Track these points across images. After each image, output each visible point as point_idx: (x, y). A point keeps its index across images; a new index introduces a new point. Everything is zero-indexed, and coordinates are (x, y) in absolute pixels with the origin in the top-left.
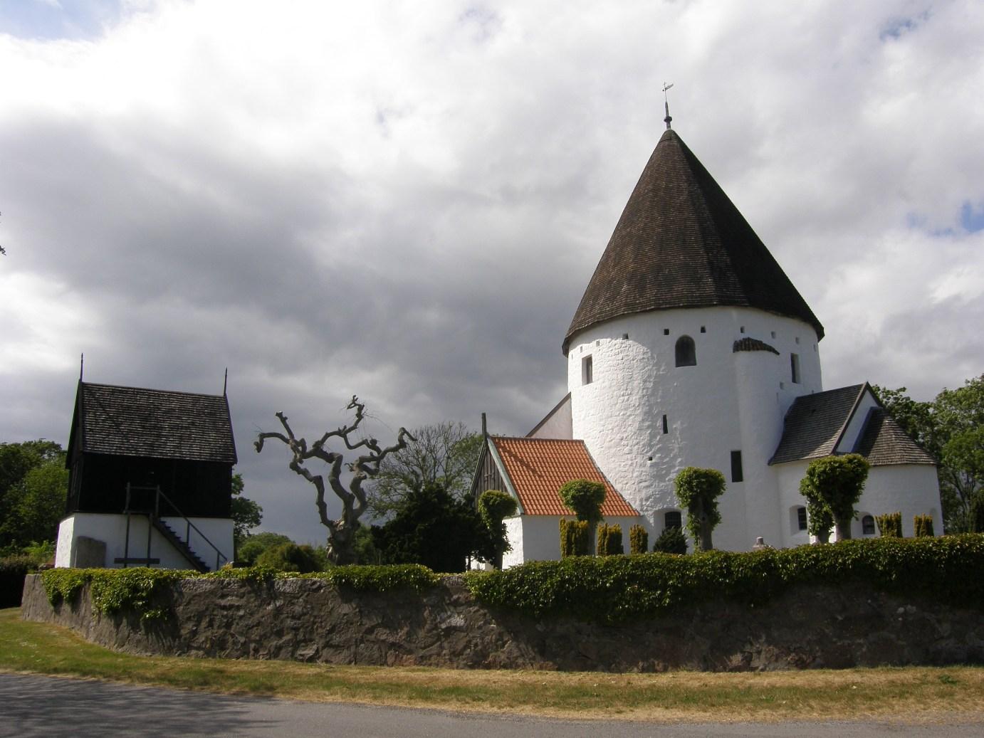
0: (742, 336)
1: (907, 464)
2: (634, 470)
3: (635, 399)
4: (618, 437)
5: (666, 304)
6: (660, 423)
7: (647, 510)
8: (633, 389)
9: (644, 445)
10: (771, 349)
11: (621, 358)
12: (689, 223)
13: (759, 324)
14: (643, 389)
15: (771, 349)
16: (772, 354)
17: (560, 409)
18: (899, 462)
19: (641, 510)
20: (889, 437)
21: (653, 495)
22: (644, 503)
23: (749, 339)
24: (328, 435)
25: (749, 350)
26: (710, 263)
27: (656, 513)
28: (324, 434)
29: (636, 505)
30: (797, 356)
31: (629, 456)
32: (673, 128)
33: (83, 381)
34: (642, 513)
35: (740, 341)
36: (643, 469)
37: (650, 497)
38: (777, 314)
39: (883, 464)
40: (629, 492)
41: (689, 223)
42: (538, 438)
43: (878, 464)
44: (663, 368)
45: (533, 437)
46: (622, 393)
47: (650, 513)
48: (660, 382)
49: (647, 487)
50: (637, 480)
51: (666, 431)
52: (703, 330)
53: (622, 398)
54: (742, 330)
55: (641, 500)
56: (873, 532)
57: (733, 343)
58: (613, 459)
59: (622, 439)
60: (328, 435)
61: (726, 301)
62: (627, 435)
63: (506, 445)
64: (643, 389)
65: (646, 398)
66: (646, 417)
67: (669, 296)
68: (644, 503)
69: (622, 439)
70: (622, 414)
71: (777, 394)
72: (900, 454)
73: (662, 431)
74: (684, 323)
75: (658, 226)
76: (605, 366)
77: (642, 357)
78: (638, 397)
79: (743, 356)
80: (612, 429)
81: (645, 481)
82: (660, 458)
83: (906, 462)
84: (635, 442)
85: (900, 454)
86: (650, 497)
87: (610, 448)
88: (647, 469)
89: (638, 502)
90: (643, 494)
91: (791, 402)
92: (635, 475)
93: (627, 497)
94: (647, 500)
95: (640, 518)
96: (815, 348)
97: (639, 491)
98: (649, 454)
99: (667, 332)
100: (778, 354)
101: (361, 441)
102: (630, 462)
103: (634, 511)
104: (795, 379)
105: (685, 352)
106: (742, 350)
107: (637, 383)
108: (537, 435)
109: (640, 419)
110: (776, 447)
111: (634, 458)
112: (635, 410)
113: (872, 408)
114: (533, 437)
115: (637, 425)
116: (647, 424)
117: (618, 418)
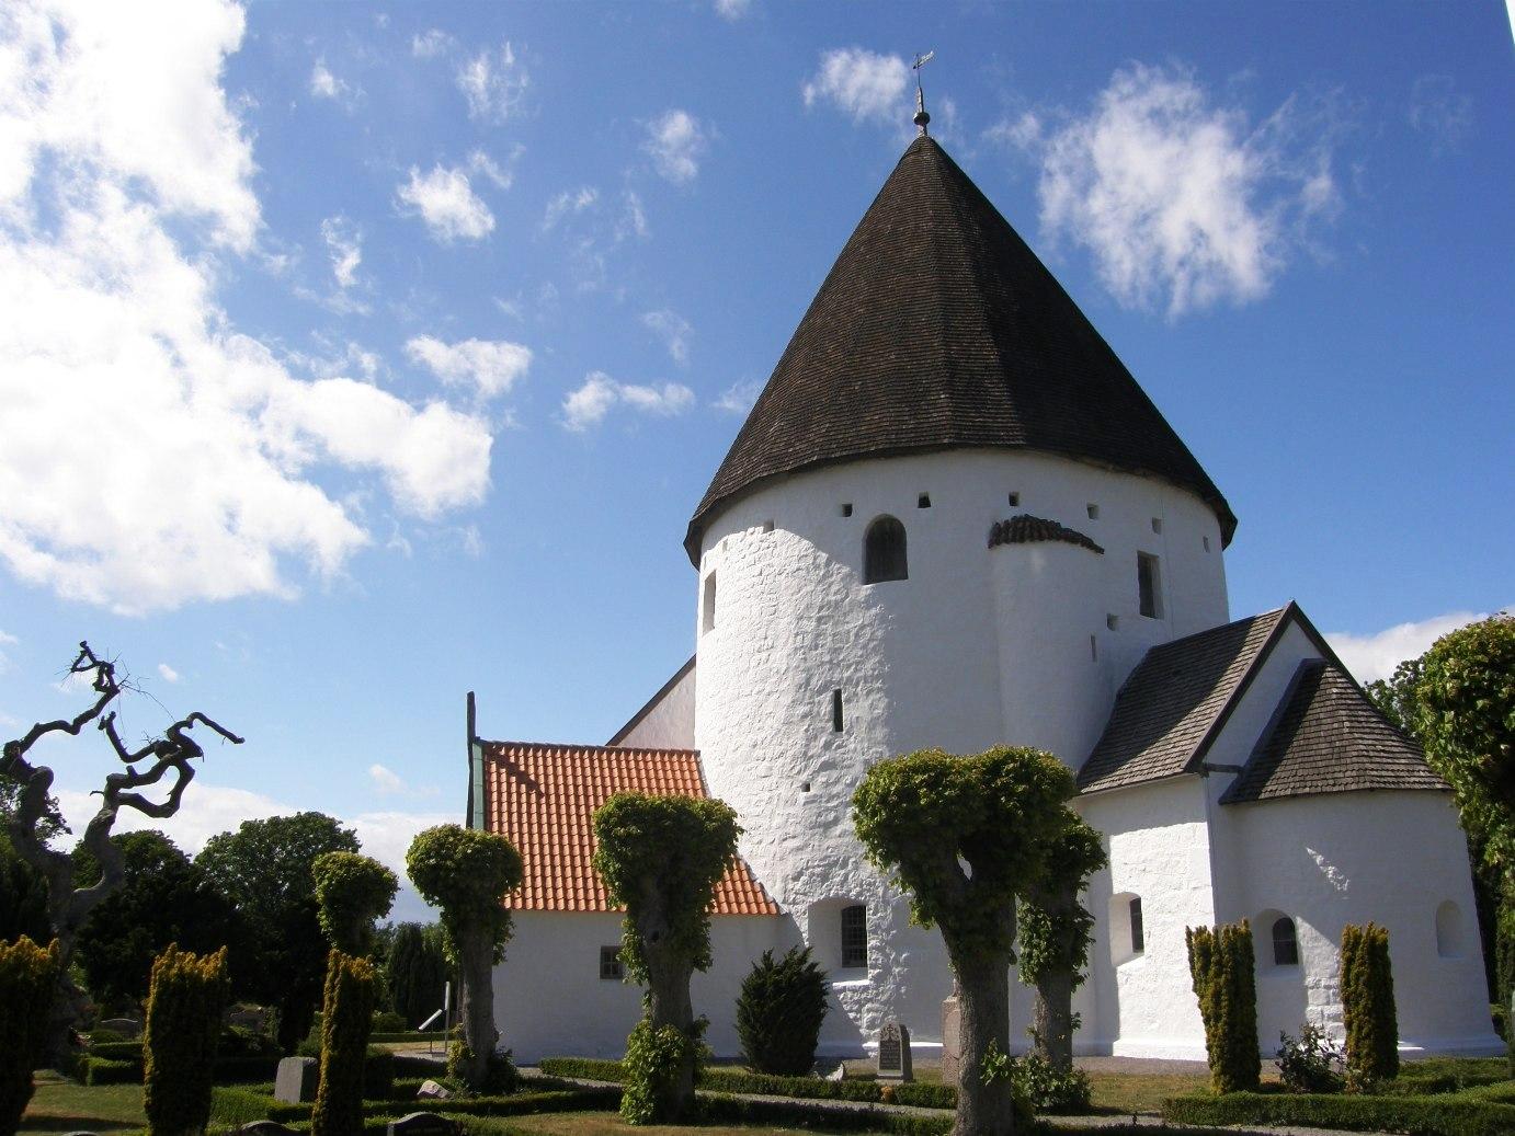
0: (1009, 513)
1: (1372, 789)
2: (773, 812)
3: (780, 659)
4: (748, 741)
5: (843, 448)
6: (826, 707)
7: (794, 903)
8: (777, 637)
9: (795, 758)
10: (1088, 543)
11: (757, 572)
12: (921, 292)
13: (1055, 487)
14: (797, 635)
15: (1088, 543)
16: (1085, 552)
17: (676, 688)
18: (1353, 787)
19: (784, 902)
20: (1336, 725)
21: (807, 868)
22: (790, 886)
23: (1027, 518)
24: (39, 730)
25: (1022, 540)
26: (951, 365)
27: (813, 908)
28: (32, 728)
29: (774, 892)
30: (1155, 558)
31: (767, 782)
32: (932, 134)
33: (485, 733)
34: (785, 909)
35: (1006, 522)
36: (792, 810)
37: (800, 874)
38: (1103, 468)
39: (1313, 790)
40: (764, 860)
41: (921, 292)
42: (628, 747)
43: (1300, 791)
44: (834, 588)
45: (621, 745)
46: (757, 646)
47: (802, 907)
48: (830, 613)
49: (799, 849)
50: (780, 832)
51: (838, 726)
52: (924, 502)
53: (758, 656)
54: (1013, 501)
55: (785, 880)
56: (139, 1047)
57: (990, 526)
58: (739, 789)
59: (755, 746)
60: (39, 730)
61: (971, 439)
62: (763, 735)
63: (522, 760)
64: (797, 635)
65: (800, 655)
66: (800, 695)
67: (852, 432)
68: (790, 886)
69: (755, 746)
70: (757, 689)
71: (1093, 638)
72: (1356, 767)
73: (830, 725)
74: (882, 490)
75: (861, 304)
76: (733, 591)
77: (795, 567)
78: (786, 652)
79: (1010, 553)
80: (739, 724)
81: (794, 837)
82: (827, 784)
83: (1368, 785)
84: (779, 749)
85: (1356, 767)
86: (800, 874)
87: (733, 765)
88: (797, 810)
89: (779, 885)
90: (789, 868)
91: (1138, 658)
92: (774, 824)
93: (759, 873)
94: (796, 879)
95: (783, 920)
96: (1221, 560)
97: (782, 859)
98: (804, 777)
99: (848, 510)
100: (1100, 550)
101: (146, 745)
102: (766, 795)
103: (767, 904)
104: (1149, 606)
105: (884, 553)
106: (1007, 541)
107: (785, 623)
108: (630, 741)
109: (787, 700)
110: (1083, 762)
111: (774, 786)
112: (780, 681)
113: (1305, 661)
114: (621, 745)
115: (781, 714)
116: (802, 709)
117: (751, 699)
